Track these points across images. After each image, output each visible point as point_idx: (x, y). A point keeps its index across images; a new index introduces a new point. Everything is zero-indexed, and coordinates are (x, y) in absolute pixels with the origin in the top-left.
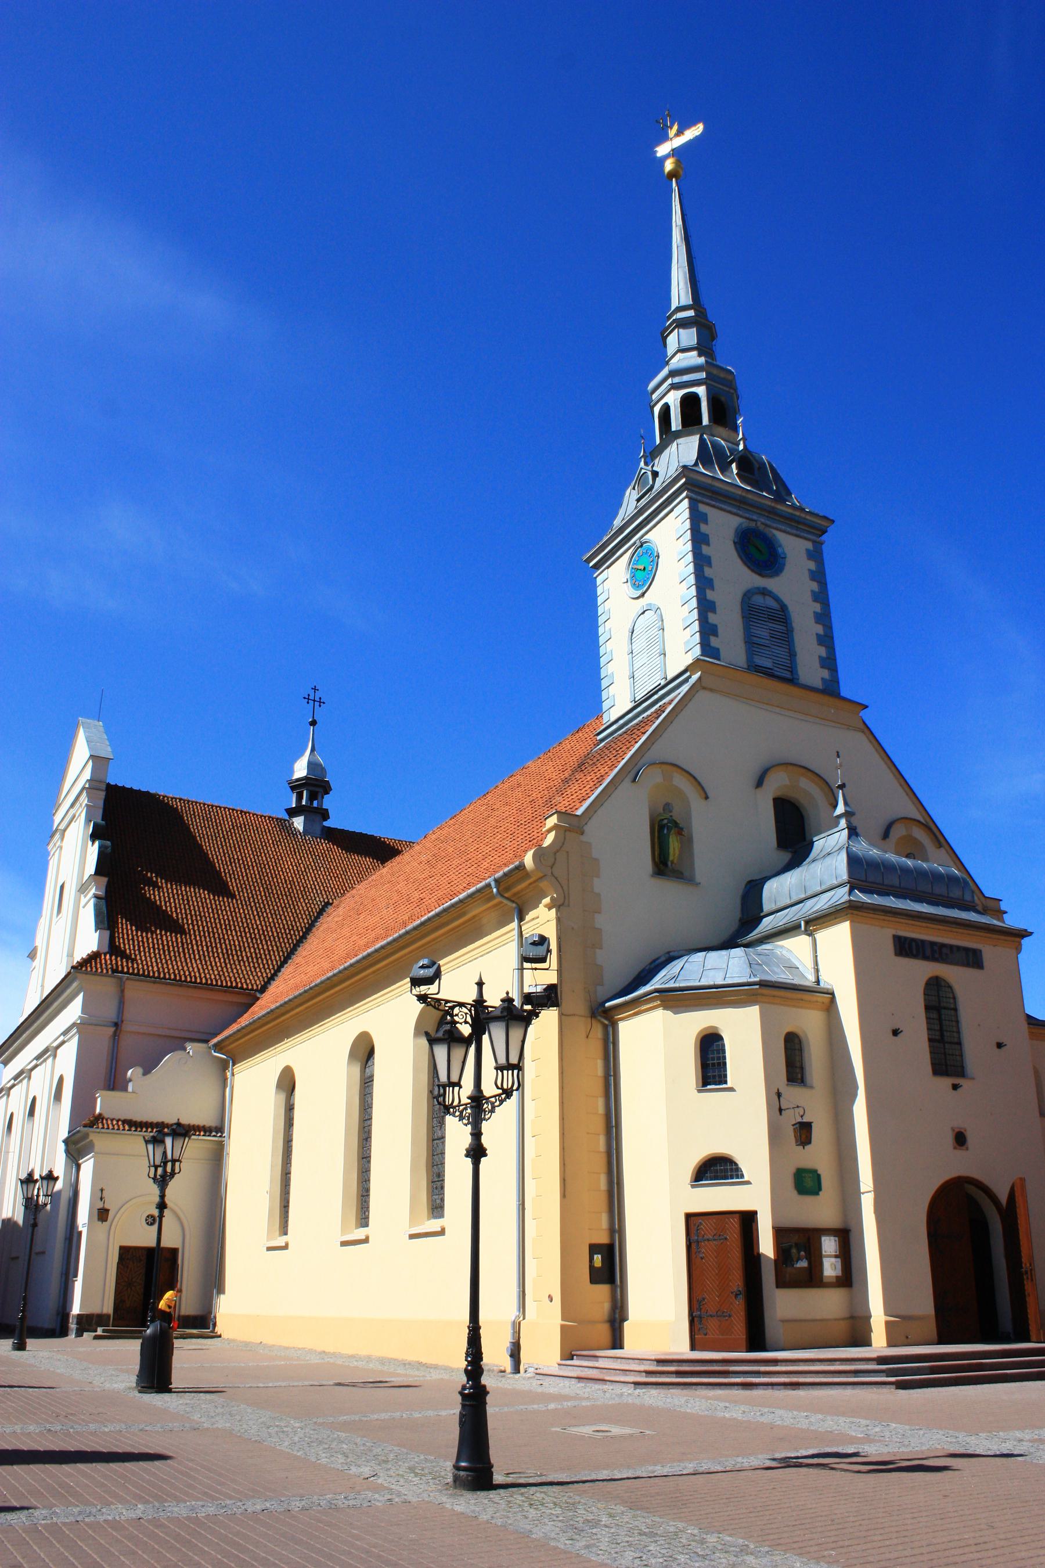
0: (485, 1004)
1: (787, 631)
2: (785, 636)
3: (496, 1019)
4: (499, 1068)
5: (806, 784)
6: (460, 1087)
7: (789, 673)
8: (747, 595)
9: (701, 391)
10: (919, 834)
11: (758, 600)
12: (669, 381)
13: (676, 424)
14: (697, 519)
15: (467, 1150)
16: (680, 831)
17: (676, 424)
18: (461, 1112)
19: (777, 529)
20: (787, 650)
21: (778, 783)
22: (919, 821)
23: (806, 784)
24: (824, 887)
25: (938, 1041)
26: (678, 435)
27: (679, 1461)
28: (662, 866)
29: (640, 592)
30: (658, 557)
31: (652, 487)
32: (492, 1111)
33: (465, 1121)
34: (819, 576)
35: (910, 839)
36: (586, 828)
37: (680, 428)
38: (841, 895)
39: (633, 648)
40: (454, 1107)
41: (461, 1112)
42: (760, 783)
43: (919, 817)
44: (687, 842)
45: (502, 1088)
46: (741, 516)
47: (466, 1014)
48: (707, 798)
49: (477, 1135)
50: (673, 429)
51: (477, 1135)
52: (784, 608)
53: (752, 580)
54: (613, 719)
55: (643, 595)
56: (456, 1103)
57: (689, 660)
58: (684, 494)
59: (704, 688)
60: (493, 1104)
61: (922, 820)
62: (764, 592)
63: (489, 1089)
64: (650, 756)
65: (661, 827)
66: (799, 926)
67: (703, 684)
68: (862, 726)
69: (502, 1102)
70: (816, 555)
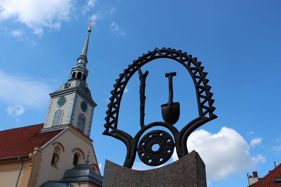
2: (84, 124)
5: (80, 153)
8: (80, 114)
9: (82, 73)
10: (95, 167)
11: (82, 116)
12: (77, 68)
13: (76, 77)
14: (76, 97)
16: (58, 157)
17: (76, 77)
19: (88, 104)
21: (77, 151)
22: (95, 165)
23: (80, 153)
24: (83, 175)
26: (75, 79)
27: (197, 177)
28: (53, 163)
30: (66, 101)
31: (68, 87)
34: (92, 115)
35: (93, 168)
36: (42, 152)
37: (76, 78)
38: (87, 179)
42: (73, 151)
44: (58, 160)
46: (83, 99)
48: (64, 151)
50: (75, 77)
52: (85, 119)
53: (82, 112)
54: (46, 128)
55: (60, 106)
57: (67, 123)
58: (75, 92)
59: (69, 130)
62: (83, 115)
64: (56, 141)
65: (55, 155)
66: (78, 182)
67: (69, 129)
70: (93, 111)
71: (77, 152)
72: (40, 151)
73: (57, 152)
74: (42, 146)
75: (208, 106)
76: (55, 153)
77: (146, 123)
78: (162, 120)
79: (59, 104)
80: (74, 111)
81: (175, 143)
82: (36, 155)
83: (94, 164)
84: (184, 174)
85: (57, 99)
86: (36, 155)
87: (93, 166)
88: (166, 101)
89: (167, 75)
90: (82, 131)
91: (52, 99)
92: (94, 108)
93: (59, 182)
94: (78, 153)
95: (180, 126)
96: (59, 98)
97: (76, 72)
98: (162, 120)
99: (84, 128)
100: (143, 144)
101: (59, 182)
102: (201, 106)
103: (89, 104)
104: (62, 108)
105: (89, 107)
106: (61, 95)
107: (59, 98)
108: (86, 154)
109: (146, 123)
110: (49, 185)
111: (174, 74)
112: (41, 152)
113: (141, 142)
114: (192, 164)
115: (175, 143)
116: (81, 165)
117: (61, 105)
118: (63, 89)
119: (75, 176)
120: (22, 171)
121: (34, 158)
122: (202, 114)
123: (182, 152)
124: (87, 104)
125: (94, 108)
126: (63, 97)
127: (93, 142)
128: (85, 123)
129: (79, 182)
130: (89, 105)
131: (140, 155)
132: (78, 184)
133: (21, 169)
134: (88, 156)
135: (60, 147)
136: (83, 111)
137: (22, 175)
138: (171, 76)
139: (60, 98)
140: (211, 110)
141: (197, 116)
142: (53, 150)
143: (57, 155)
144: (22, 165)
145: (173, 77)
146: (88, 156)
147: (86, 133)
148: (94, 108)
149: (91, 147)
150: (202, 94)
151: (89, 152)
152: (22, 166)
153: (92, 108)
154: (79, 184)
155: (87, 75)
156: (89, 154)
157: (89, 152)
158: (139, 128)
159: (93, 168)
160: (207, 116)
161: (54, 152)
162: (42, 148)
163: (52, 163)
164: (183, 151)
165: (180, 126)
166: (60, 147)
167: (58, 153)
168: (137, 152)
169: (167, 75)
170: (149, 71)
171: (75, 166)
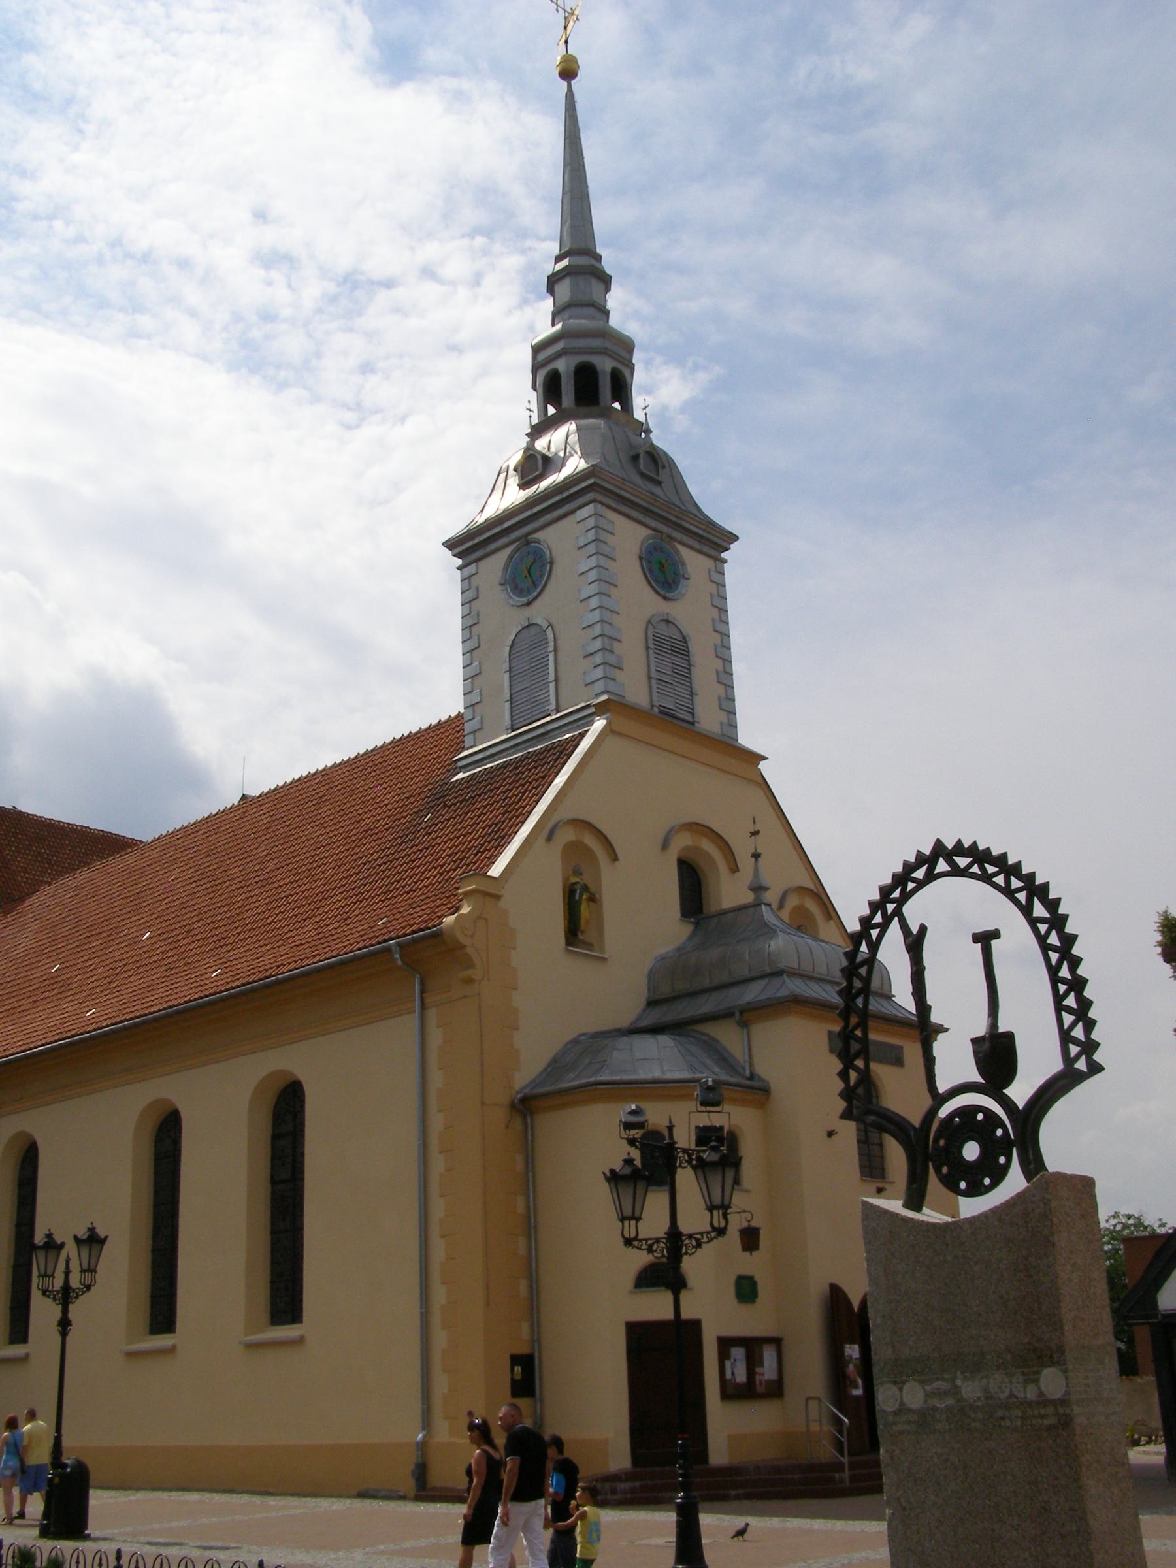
0: (676, 1145)
1: (689, 665)
2: (684, 673)
3: (40, 1248)
4: (83, 1271)
5: (707, 846)
6: (54, 1277)
7: (690, 715)
10: (812, 906)
11: (664, 630)
15: (59, 1322)
16: (592, 899)
18: (55, 1296)
19: (684, 544)
20: (688, 693)
21: (683, 841)
22: (812, 890)
23: (707, 846)
25: (864, 1143)
28: (573, 933)
29: (524, 600)
30: (552, 563)
32: (77, 1297)
33: (58, 1302)
35: (800, 911)
39: (512, 665)
40: (50, 1291)
41: (55, 1296)
42: (665, 846)
43: (812, 886)
45: (84, 1284)
47: (663, 1248)
49: (65, 1311)
51: (65, 1311)
55: (529, 604)
56: (50, 1289)
60: (77, 1293)
61: (815, 890)
63: (75, 1282)
64: (564, 814)
68: (760, 780)
69: (83, 1293)
71: (689, 843)
72: (493, 891)
73: (577, 872)
74: (491, 861)
75: (1082, 1037)
76: (573, 880)
77: (942, 1086)
78: (978, 1078)
79: (518, 590)
80: (615, 644)
81: (1012, 1137)
82: (479, 917)
83: (802, 890)
84: (1027, 1227)
85: (495, 565)
86: (477, 917)
87: (792, 902)
88: (981, 1030)
89: (977, 938)
90: (688, 718)
91: (468, 571)
92: (725, 561)
93: (634, 1031)
94: (697, 849)
95: (1020, 1092)
96: (507, 552)
97: (561, 365)
98: (978, 1078)
99: (692, 694)
100: (942, 1143)
101: (634, 1031)
102: (1066, 1037)
103: (691, 548)
104: (539, 613)
105: (693, 561)
106: (513, 536)
107: (507, 552)
108: (742, 848)
109: (942, 1086)
110: (587, 1061)
111: (996, 934)
112: (498, 897)
113: (936, 1140)
114: (1042, 1205)
115: (1012, 1137)
116: (725, 912)
117: (529, 592)
118: (514, 495)
119: (707, 983)
120: (432, 1014)
121: (472, 937)
122: (1068, 1060)
123: (1030, 1163)
124: (677, 551)
125: (724, 555)
126: (526, 541)
127: (762, 766)
128: (689, 666)
129: (741, 1013)
130: (693, 553)
131: (938, 1170)
132: (739, 1023)
133: (423, 1007)
134: (756, 856)
135: (590, 841)
136: (665, 598)
137: (436, 1037)
138: (985, 939)
139: (511, 557)
140: (1090, 1047)
141: (1057, 1065)
142: (558, 865)
143: (586, 888)
144: (422, 983)
145: (994, 943)
146: (756, 856)
147: (708, 720)
148: (725, 561)
149: (760, 793)
150: (1065, 1003)
151: (755, 833)
152: (423, 991)
153: (710, 563)
154: (744, 1024)
155: (632, 368)
156: (761, 844)
157: (755, 833)
158: (928, 1102)
159: (800, 911)
160: (1081, 1065)
161: (566, 880)
162: (496, 870)
163: (569, 942)
164: (1033, 1164)
165: (1020, 1092)
166: (590, 841)
167: (587, 879)
168: (930, 1164)
169: (977, 938)
170: (927, 925)
171: (697, 924)
